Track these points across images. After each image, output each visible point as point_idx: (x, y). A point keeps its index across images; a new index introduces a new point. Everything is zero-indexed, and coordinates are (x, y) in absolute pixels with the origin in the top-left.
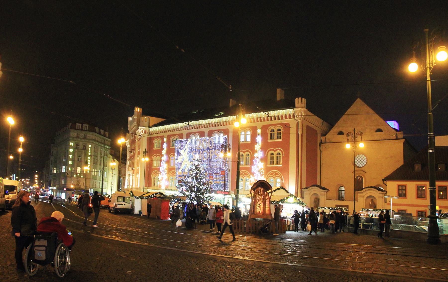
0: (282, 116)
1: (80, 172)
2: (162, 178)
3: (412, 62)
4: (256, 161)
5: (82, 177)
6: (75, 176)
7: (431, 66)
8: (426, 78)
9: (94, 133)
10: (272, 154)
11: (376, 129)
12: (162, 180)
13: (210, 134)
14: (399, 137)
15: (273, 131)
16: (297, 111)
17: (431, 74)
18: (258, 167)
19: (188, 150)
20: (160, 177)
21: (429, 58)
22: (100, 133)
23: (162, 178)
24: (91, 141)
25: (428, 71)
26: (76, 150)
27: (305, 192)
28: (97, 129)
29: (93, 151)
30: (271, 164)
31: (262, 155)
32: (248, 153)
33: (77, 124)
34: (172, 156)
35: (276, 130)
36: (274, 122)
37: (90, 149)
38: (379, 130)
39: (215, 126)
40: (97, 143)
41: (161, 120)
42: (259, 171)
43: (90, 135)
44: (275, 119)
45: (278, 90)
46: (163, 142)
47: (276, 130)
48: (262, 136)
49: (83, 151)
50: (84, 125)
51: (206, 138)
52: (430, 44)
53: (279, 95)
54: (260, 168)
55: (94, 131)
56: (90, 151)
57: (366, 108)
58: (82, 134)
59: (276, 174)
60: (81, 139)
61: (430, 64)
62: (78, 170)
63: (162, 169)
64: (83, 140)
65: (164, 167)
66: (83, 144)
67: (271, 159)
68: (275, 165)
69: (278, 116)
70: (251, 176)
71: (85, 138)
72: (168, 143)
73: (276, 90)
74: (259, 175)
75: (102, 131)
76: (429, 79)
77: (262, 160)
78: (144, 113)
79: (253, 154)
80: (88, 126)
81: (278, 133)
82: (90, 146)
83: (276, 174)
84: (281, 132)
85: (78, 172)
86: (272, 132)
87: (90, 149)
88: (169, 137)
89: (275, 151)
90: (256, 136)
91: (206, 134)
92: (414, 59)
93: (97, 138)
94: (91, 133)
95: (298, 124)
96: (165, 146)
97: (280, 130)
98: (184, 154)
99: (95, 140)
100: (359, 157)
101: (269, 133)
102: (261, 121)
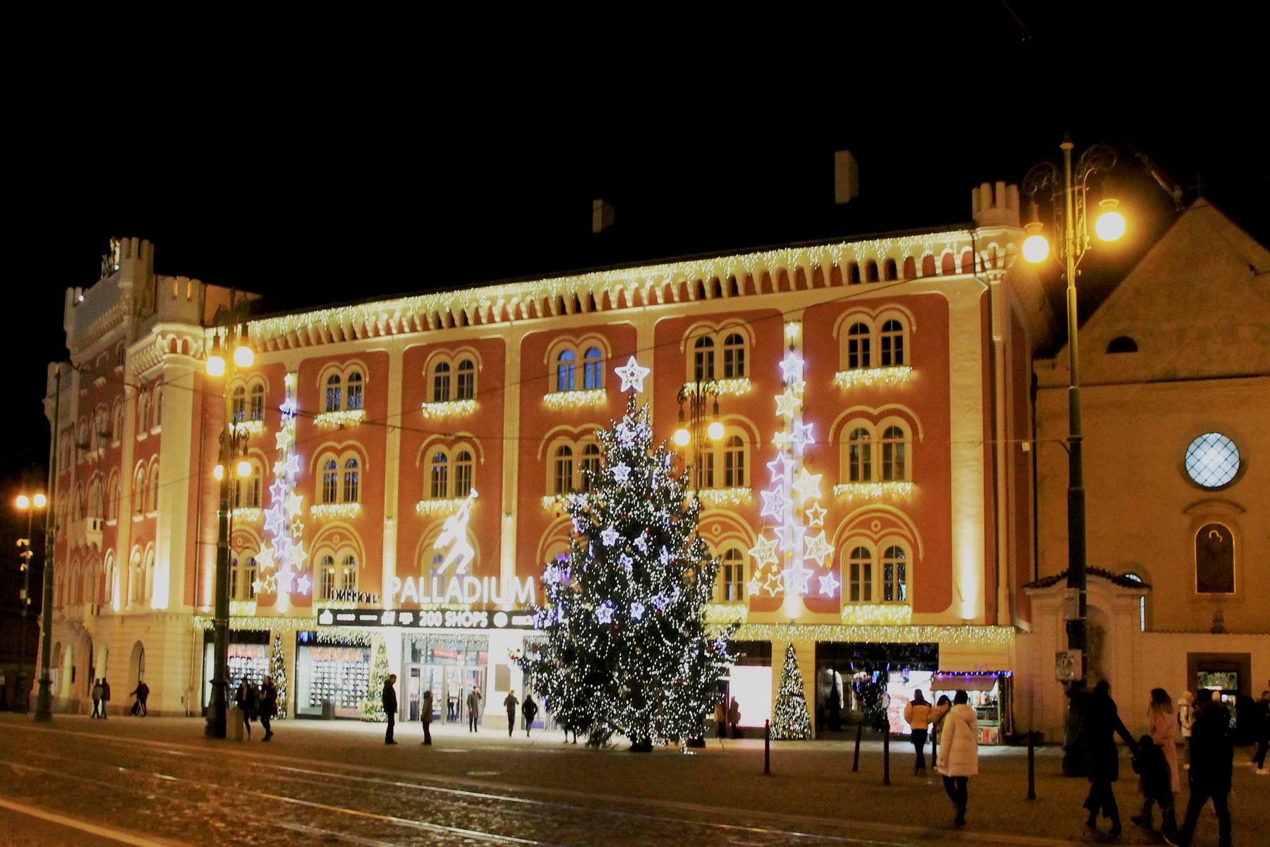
0: (733, 281)
2: (279, 561)
4: (781, 469)
8: (1065, 284)
10: (566, 451)
12: (272, 572)
15: (709, 342)
16: (986, 242)
18: (285, 512)
21: (1074, 228)
23: (279, 561)
27: (1035, 603)
31: (297, 470)
32: (465, 447)
35: (454, 365)
36: (864, 289)
39: (331, 341)
42: (287, 528)
44: (577, 309)
46: (772, 348)
47: (454, 365)
48: (806, 354)
54: (803, 500)
67: (560, 473)
69: (800, 272)
70: (263, 546)
76: (1072, 290)
78: (165, 265)
79: (272, 466)
81: (461, 378)
84: (746, 346)
86: (442, 374)
89: (875, 420)
90: (781, 356)
97: (469, 365)
101: (431, 376)
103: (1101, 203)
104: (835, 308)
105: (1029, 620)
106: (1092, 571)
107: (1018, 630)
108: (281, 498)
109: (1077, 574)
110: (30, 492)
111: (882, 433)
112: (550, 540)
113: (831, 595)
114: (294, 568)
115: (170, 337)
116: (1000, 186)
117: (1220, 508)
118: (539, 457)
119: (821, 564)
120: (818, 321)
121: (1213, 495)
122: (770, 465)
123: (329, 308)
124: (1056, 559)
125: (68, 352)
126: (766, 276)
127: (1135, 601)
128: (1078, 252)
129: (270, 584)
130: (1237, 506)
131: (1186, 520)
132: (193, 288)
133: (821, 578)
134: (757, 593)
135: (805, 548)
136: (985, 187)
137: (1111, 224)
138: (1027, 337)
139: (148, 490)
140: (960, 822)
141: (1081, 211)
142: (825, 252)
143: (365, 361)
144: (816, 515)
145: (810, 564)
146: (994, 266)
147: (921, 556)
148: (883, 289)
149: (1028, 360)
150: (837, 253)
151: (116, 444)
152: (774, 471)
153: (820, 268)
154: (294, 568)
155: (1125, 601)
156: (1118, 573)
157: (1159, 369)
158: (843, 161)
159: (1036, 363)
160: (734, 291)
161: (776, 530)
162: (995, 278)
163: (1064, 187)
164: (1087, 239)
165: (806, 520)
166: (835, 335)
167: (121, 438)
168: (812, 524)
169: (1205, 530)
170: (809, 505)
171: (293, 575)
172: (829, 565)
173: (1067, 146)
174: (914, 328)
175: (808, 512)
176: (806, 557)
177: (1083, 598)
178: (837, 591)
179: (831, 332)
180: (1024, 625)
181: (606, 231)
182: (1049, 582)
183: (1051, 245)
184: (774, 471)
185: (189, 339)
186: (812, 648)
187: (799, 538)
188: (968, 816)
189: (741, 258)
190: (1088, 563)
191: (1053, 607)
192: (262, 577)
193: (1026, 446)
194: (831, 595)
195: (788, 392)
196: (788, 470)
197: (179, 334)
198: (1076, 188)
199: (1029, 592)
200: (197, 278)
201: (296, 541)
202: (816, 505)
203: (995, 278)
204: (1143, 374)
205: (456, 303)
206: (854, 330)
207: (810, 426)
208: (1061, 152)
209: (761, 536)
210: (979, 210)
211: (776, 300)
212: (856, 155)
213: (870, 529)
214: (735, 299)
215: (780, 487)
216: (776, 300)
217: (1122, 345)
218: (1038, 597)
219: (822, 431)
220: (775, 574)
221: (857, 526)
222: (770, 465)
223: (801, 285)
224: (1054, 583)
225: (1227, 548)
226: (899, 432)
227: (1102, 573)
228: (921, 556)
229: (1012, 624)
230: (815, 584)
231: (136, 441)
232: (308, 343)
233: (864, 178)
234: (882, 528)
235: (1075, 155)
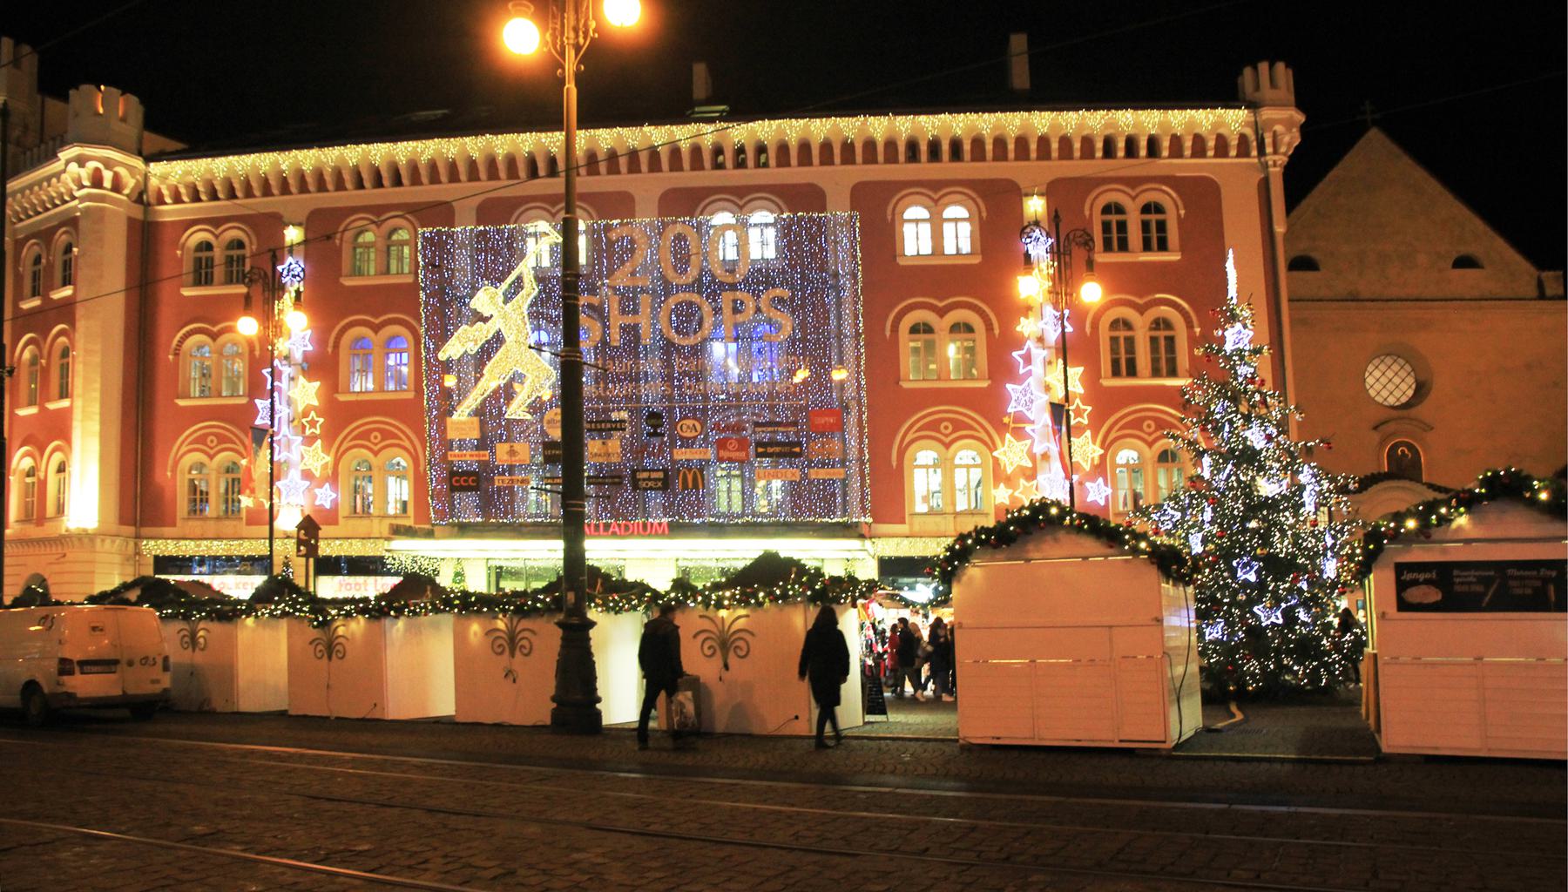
4: (1028, 359)
7: (581, 41)
8: (562, 82)
11: (1455, 255)
13: (686, 202)
14: (1549, 292)
17: (578, 68)
19: (531, 290)
25: (570, 54)
36: (1120, 165)
38: (1464, 262)
45: (1018, 43)
57: (1407, 169)
59: (386, 435)
73: (1005, 42)
74: (300, 439)
83: (958, 425)
89: (942, 313)
95: (1265, 185)
100: (1403, 374)
102: (303, 188)
104: (1088, 185)
112: (184, 449)
113: (1102, 503)
115: (92, 165)
118: (888, 333)
120: (1062, 194)
123: (1052, 110)
132: (126, 104)
136: (1263, 67)
139: (46, 371)
142: (1084, 118)
143: (591, 204)
145: (307, 475)
146: (1275, 152)
148: (1142, 166)
153: (852, 143)
162: (1275, 165)
166: (1087, 213)
168: (308, 432)
174: (1182, 212)
178: (335, 503)
179: (1082, 211)
185: (122, 171)
194: (1102, 503)
196: (285, 377)
197: (108, 163)
200: (134, 93)
201: (310, 441)
203: (1275, 165)
205: (276, 164)
206: (1107, 209)
210: (1257, 88)
211: (276, 203)
213: (1141, 430)
215: (1030, 380)
216: (276, 203)
221: (355, 438)
226: (1168, 325)
234: (954, 431)
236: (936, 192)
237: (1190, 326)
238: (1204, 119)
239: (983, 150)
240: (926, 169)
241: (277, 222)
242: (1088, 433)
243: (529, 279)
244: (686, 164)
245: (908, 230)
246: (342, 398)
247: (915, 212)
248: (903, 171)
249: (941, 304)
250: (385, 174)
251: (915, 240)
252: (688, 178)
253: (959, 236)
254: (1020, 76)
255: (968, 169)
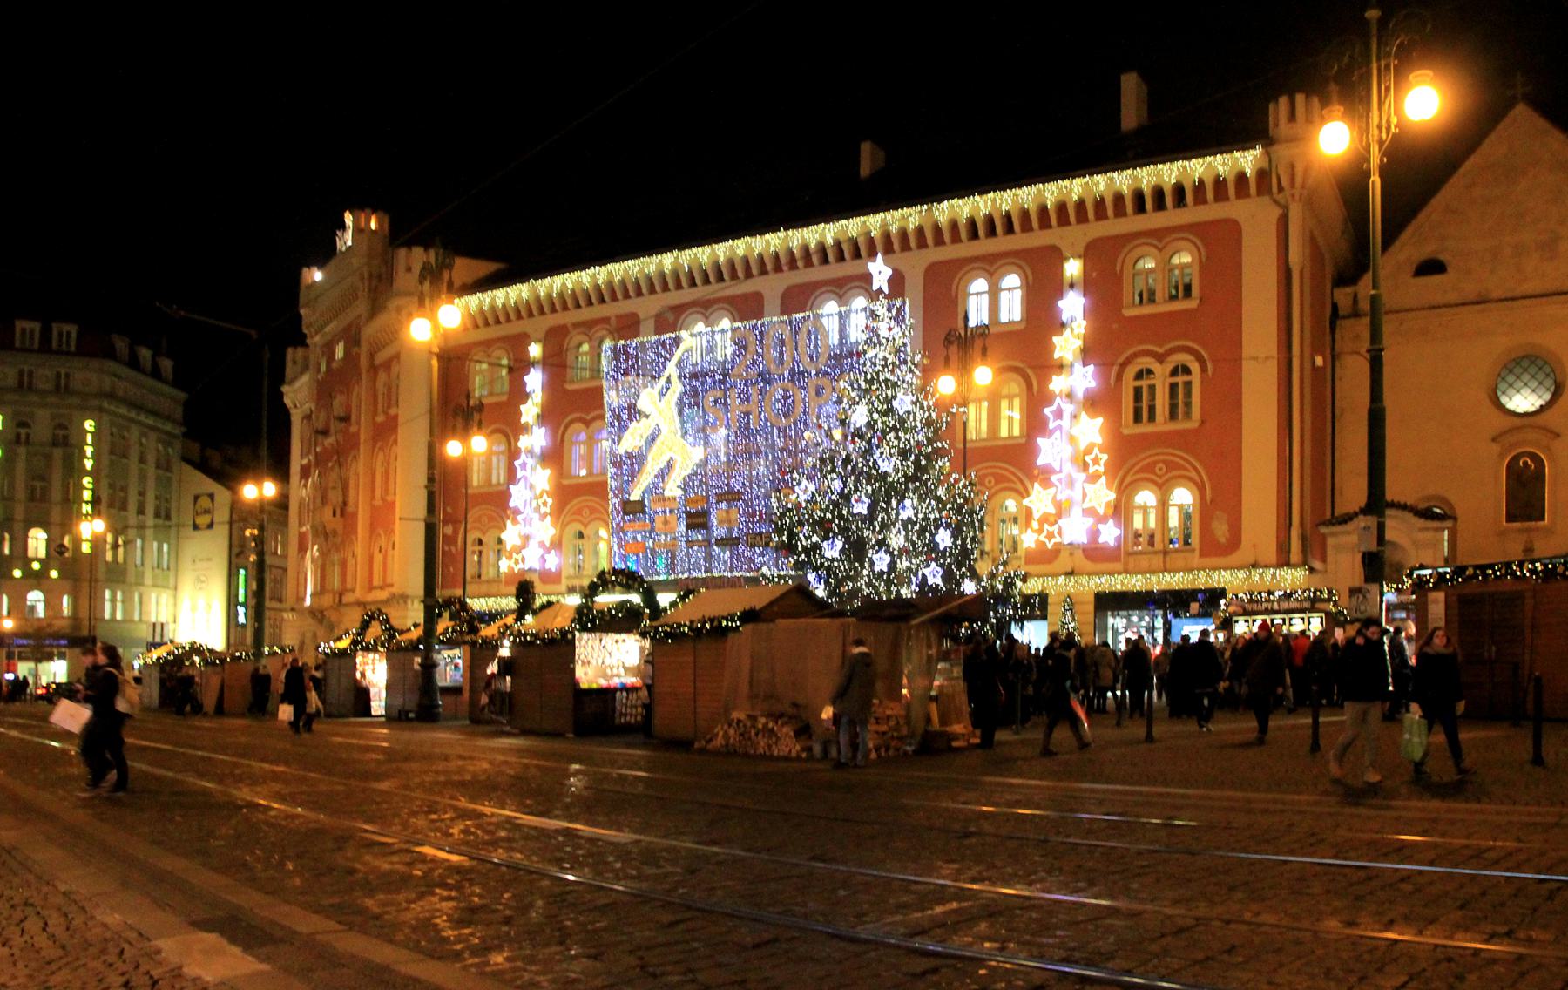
1: (42, 554)
2: (526, 538)
3: (1331, 119)
4: (1059, 414)
5: (54, 574)
6: (17, 573)
8: (1367, 175)
9: (112, 365)
13: (798, 299)
18: (531, 487)
19: (677, 388)
20: (511, 535)
21: (1380, 109)
22: (134, 363)
23: (526, 538)
24: (95, 402)
26: (22, 450)
27: (1331, 541)
28: (121, 345)
29: (106, 448)
30: (1137, 418)
31: (1093, 384)
33: (20, 325)
34: (578, 426)
37: (89, 438)
40: (123, 410)
41: (485, 268)
43: (88, 374)
46: (520, 366)
49: (58, 453)
50: (55, 327)
51: (773, 319)
52: (1383, 63)
53: (868, 159)
54: (1082, 446)
55: (110, 354)
56: (89, 450)
58: (45, 372)
60: (43, 393)
61: (1380, 127)
62: (31, 543)
63: (519, 496)
64: (52, 399)
65: (533, 485)
66: (53, 417)
68: (1162, 424)
69: (972, 222)
70: (509, 523)
71: (62, 388)
72: (555, 364)
75: (145, 353)
76: (1375, 179)
77: (1092, 403)
78: (401, 234)
79: (517, 440)
80: (73, 329)
82: (89, 425)
83: (1170, 466)
85: (31, 554)
87: (89, 438)
88: (556, 341)
89: (1161, 358)
90: (1060, 294)
91: (772, 301)
92: (1338, 109)
93: (122, 387)
94: (95, 363)
96: (534, 380)
98: (659, 405)
99: (111, 396)
103: (1411, 77)
105: (1324, 560)
106: (1393, 505)
107: (1311, 570)
108: (528, 473)
109: (1376, 503)
110: (258, 480)
111: (1168, 371)
114: (542, 544)
116: (1300, 98)
117: (1532, 435)
119: (1101, 511)
121: (1526, 421)
122: (1047, 411)
124: (1354, 492)
125: (305, 336)
126: (1043, 210)
127: (1438, 535)
128: (1384, 136)
129: (1050, 536)
130: (1552, 432)
131: (1495, 448)
133: (1101, 527)
134: (1033, 546)
135: (1085, 495)
136: (1283, 101)
137: (1424, 102)
138: (1327, 256)
140: (1261, 741)
141: (1388, 89)
144: (1096, 461)
147: (1208, 498)
149: (1329, 285)
150: (1123, 180)
151: (353, 429)
152: (1051, 417)
153: (1102, 199)
154: (542, 544)
155: (1429, 535)
156: (1422, 506)
157: (1470, 289)
158: (1130, 84)
159: (1336, 291)
160: (1009, 228)
161: (1054, 478)
163: (1369, 63)
164: (1394, 120)
165: (1085, 466)
167: (358, 423)
169: (1516, 458)
170: (1088, 451)
171: (541, 551)
172: (1111, 511)
173: (1373, 14)
175: (1088, 459)
176: (1087, 505)
177: (1381, 528)
180: (1317, 565)
181: (874, 176)
182: (1347, 519)
183: (1352, 129)
184: (1051, 417)
186: (1092, 599)
187: (1078, 485)
188: (1270, 735)
189: (1018, 191)
190: (1389, 497)
191: (1344, 554)
192: (509, 558)
193: (1319, 361)
195: (1067, 332)
196: (1066, 416)
198: (1383, 63)
199: (1323, 530)
202: (1096, 450)
204: (1453, 297)
205: (579, 282)
207: (1091, 368)
208: (1367, 23)
209: (1036, 485)
210: (1277, 125)
211: (1234, 209)
212: (1145, 77)
214: (1141, 217)
215: (1057, 433)
217: (1431, 267)
218: (1333, 534)
219: (1103, 374)
220: (1051, 525)
222: (1047, 411)
223: (922, 244)
224: (1351, 519)
225: (1539, 476)
226: (1187, 371)
227: (1403, 507)
228: (1208, 498)
229: (1304, 563)
230: (1094, 534)
231: (374, 423)
232: (554, 310)
233: (1155, 102)
235: (1383, 22)
236: (991, 266)
237: (1204, 369)
238: (1221, 164)
239: (1067, 216)
240: (985, 246)
241: (521, 341)
242: (1103, 479)
243: (674, 379)
244: (1035, 224)
245: (972, 303)
246: (566, 482)
247: (980, 285)
248: (966, 249)
249: (1161, 351)
250: (656, 283)
251: (977, 311)
252: (802, 276)
253: (1012, 308)
254: (1132, 110)
255: (1019, 241)
